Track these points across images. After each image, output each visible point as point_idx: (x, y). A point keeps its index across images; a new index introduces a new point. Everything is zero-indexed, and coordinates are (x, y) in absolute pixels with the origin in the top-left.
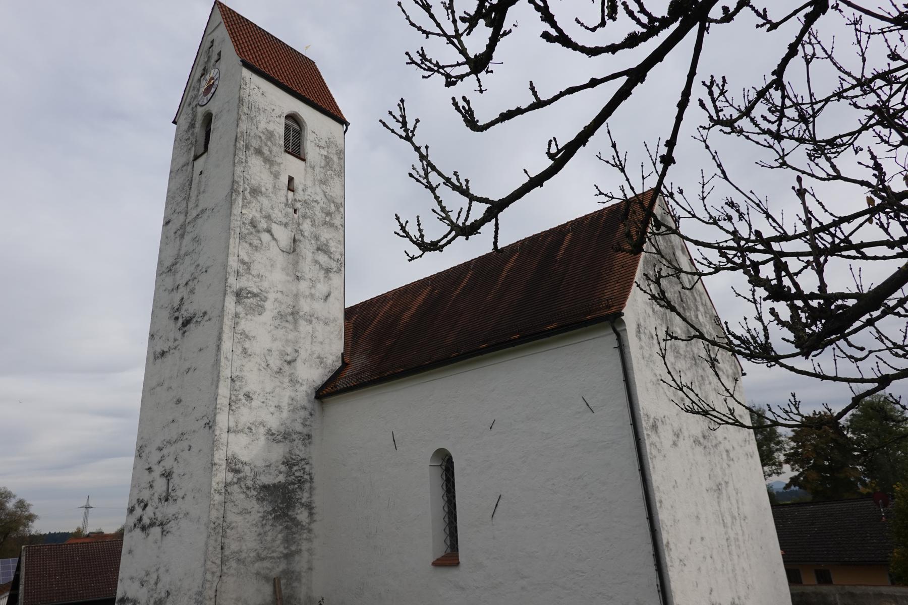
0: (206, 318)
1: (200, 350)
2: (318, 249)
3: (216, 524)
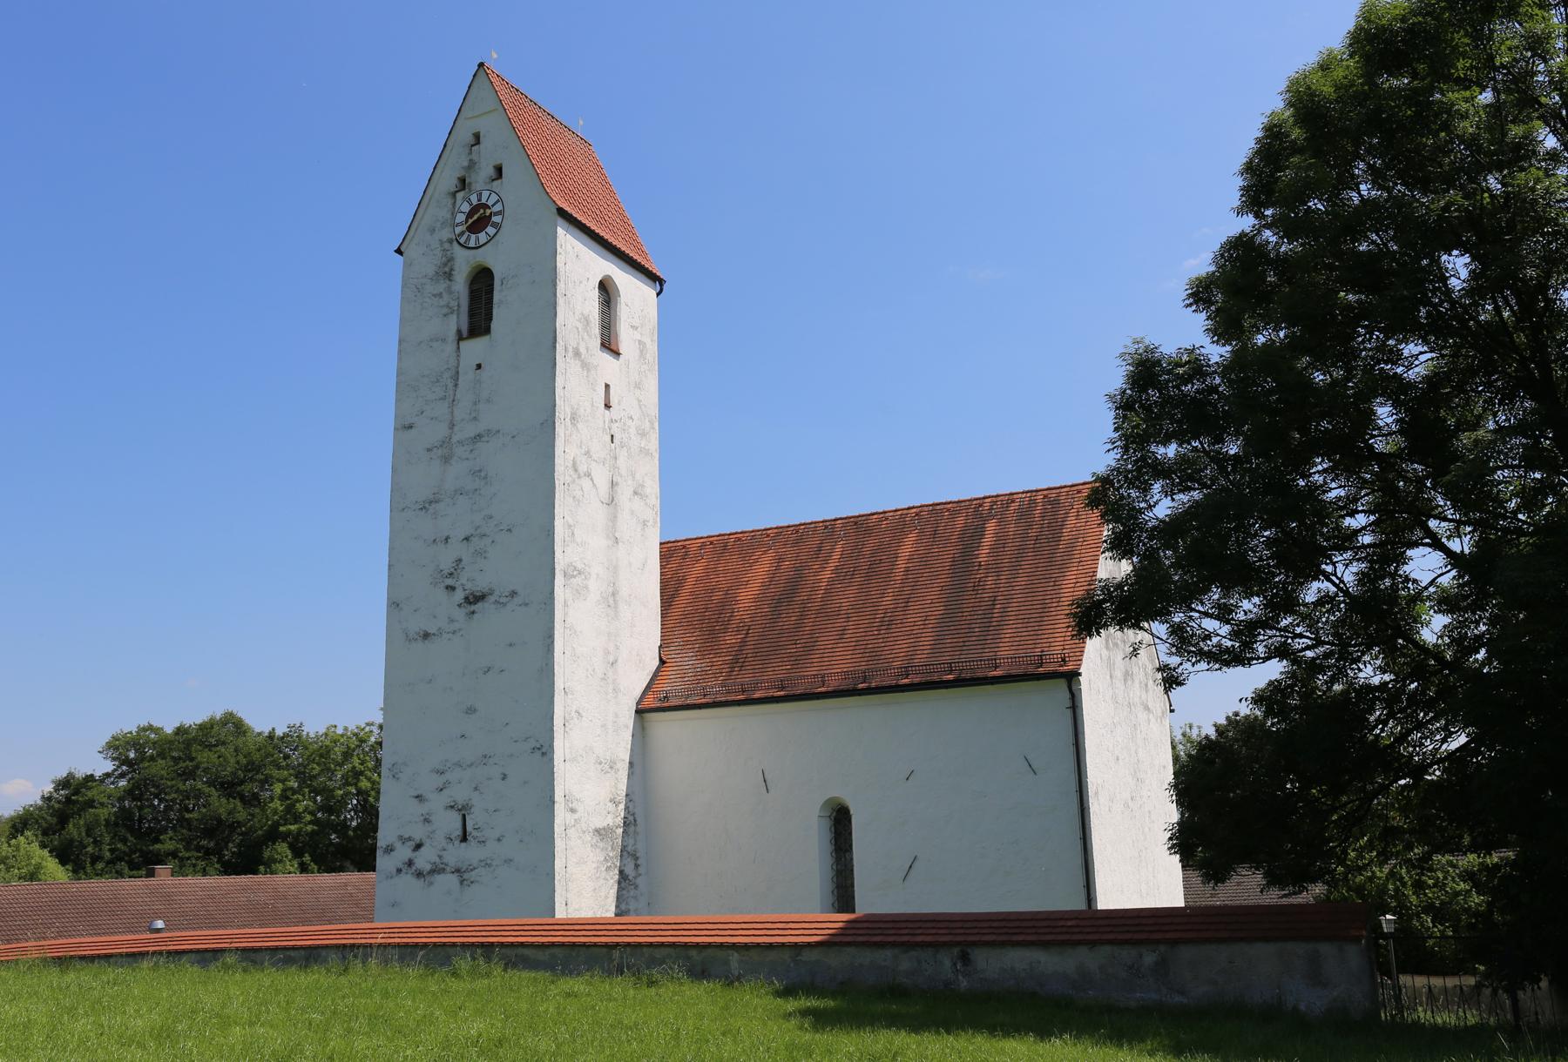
0: (517, 600)
2: (635, 493)
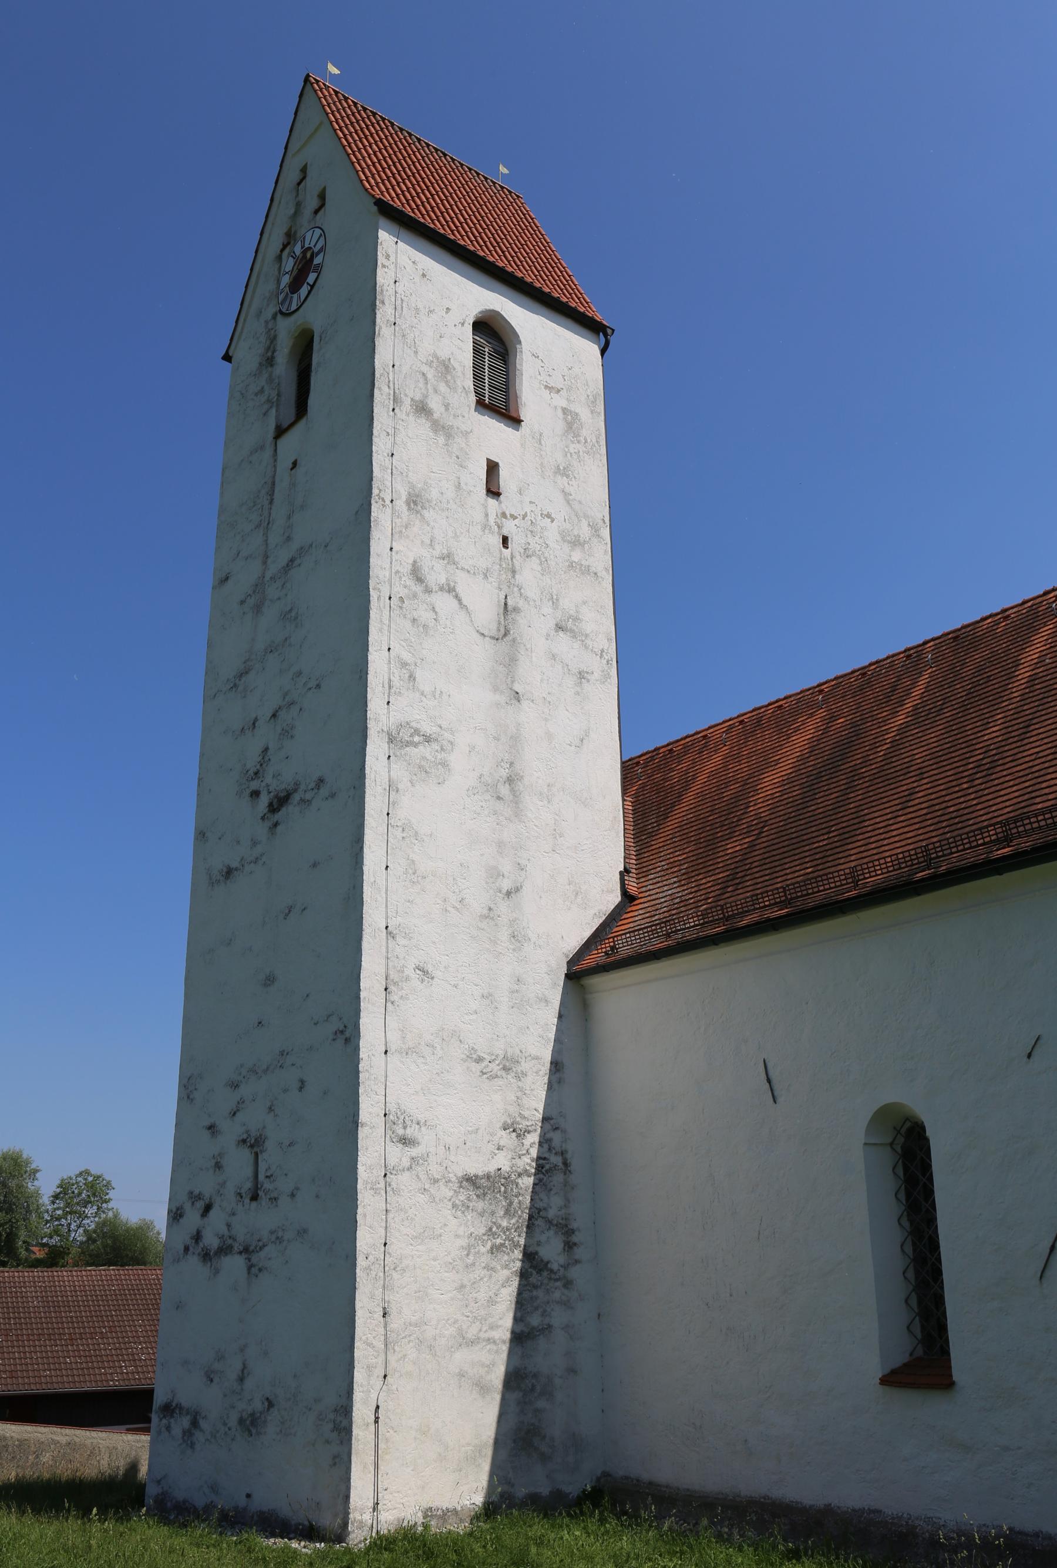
0: (324, 791)
1: (315, 865)
2: (559, 628)
3: (371, 1258)
